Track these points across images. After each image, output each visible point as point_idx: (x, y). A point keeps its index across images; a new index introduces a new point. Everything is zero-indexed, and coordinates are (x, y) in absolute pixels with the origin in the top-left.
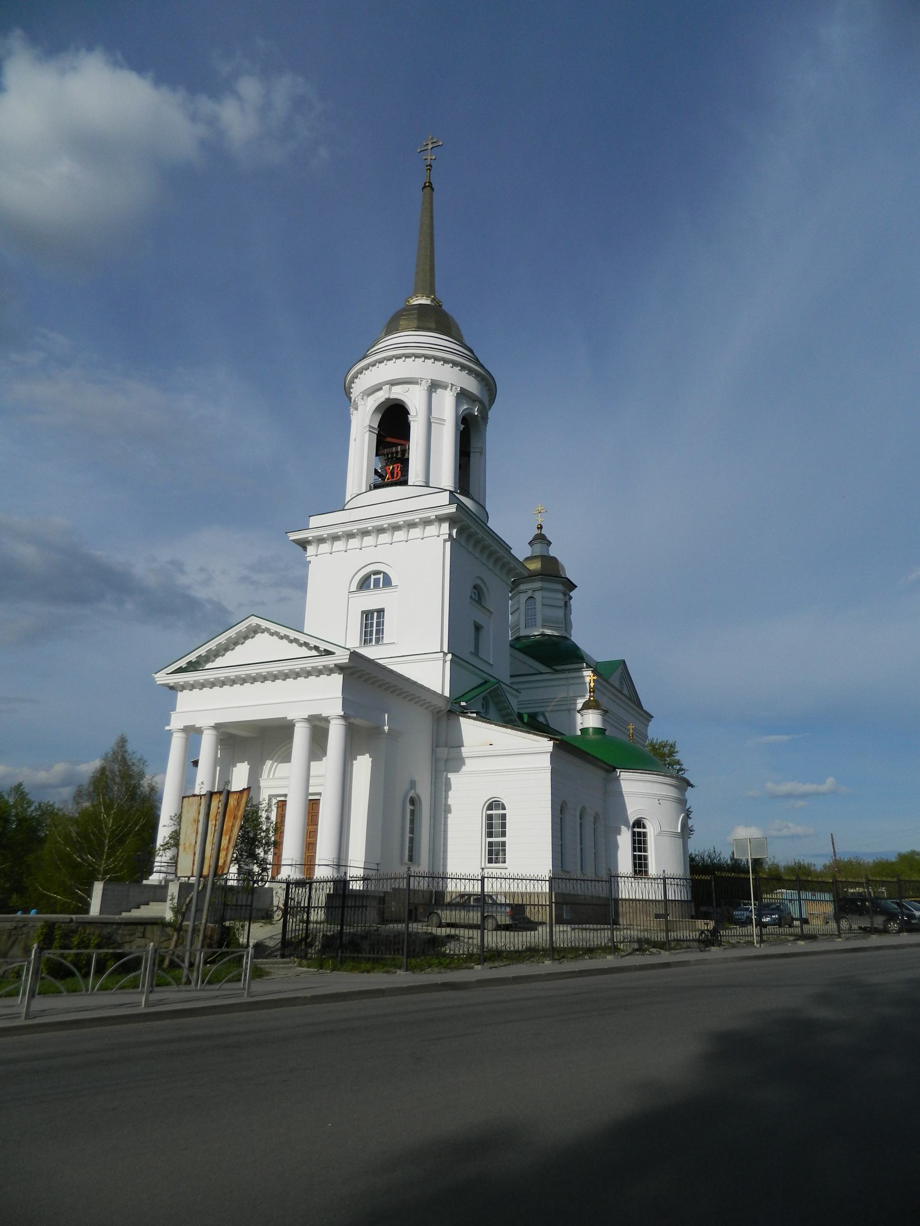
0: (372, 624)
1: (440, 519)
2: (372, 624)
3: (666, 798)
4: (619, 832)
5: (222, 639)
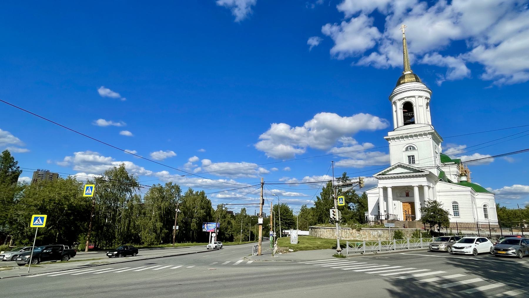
0: (412, 159)
1: (429, 134)
2: (412, 159)
5: (388, 169)
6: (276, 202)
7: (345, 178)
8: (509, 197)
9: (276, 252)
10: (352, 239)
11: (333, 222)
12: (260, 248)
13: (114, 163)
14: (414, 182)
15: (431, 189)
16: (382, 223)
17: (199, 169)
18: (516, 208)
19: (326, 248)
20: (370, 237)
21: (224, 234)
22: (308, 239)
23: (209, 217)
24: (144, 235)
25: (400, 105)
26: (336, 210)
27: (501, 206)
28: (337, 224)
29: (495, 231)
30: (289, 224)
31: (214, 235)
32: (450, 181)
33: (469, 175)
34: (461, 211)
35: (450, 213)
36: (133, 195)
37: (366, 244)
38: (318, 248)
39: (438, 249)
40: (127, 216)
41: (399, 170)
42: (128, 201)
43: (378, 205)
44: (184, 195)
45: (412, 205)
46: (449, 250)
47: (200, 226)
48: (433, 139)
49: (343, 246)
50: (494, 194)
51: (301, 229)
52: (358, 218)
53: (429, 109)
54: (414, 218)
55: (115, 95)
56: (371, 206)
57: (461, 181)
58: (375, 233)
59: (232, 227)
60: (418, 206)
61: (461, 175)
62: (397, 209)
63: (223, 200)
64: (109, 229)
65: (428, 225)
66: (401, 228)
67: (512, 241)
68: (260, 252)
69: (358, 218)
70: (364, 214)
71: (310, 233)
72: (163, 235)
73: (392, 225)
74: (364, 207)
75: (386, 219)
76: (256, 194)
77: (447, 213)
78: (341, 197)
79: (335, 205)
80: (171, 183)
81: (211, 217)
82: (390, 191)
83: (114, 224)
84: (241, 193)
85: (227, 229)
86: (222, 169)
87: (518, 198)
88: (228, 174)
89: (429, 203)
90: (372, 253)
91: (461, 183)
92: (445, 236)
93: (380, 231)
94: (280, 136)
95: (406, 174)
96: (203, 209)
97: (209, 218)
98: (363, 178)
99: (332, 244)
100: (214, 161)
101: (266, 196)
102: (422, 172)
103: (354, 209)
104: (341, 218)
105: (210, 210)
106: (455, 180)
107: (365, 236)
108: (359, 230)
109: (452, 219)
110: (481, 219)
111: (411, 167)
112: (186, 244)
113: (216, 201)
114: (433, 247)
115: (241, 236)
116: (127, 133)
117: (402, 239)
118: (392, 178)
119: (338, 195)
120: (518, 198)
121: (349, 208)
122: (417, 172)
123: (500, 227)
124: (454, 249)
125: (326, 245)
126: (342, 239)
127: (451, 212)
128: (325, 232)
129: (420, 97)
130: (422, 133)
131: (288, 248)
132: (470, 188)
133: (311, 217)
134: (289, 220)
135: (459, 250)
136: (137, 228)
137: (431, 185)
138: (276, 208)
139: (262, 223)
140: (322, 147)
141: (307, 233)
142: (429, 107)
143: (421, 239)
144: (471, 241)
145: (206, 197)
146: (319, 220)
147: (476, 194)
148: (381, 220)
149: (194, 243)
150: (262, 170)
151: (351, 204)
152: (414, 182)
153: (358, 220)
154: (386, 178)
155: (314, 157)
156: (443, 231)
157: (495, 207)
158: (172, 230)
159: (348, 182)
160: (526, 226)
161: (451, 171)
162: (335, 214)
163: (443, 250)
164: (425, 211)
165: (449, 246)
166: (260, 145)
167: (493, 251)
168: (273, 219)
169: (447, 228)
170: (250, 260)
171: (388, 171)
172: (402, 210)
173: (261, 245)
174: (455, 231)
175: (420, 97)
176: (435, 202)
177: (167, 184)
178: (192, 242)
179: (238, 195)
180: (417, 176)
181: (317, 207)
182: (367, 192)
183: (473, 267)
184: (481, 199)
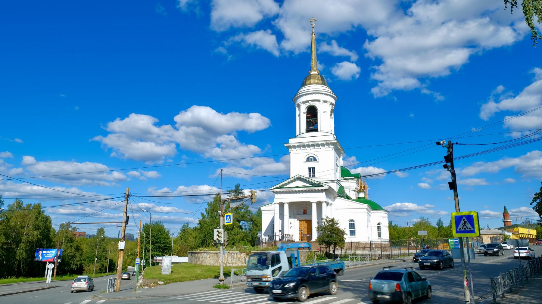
0: (312, 171)
1: (332, 144)
2: (312, 171)
3: (337, 224)
5: (286, 182)
6: (146, 220)
7: (237, 190)
9: (141, 286)
10: (240, 265)
11: (217, 245)
12: (118, 281)
14: (313, 198)
17: (20, 170)
18: (406, 226)
19: (206, 277)
21: (69, 265)
22: (185, 267)
23: (46, 240)
25: (304, 109)
26: (222, 230)
27: (393, 224)
28: (221, 247)
29: (386, 250)
31: (51, 266)
32: (348, 198)
33: (367, 191)
35: (346, 233)
38: (197, 278)
41: (299, 183)
43: (272, 223)
45: (309, 223)
49: (227, 275)
50: (388, 212)
52: (250, 239)
53: (333, 116)
54: (311, 238)
56: (265, 225)
57: (359, 198)
59: (81, 255)
60: (315, 225)
61: (359, 191)
62: (293, 228)
63: (66, 217)
65: (324, 246)
76: (116, 209)
77: (343, 232)
78: (229, 214)
79: (221, 224)
81: (49, 240)
82: (286, 207)
84: (92, 207)
85: (73, 257)
87: (405, 215)
89: (326, 221)
91: (359, 200)
94: (135, 131)
96: (37, 229)
97: (47, 242)
98: (256, 192)
99: (215, 271)
100: (39, 159)
102: (322, 186)
103: (246, 229)
104: (226, 240)
105: (49, 231)
106: (353, 197)
109: (348, 239)
110: (375, 239)
111: (311, 181)
112: (6, 280)
113: (58, 217)
115: (95, 266)
118: (290, 192)
119: (226, 211)
120: (405, 215)
121: (241, 227)
122: (316, 186)
123: (391, 246)
125: (206, 274)
126: (228, 265)
127: (347, 231)
128: (208, 258)
129: (325, 102)
130: (325, 142)
131: (157, 280)
132: (366, 206)
133: (192, 239)
134: (163, 243)
137: (330, 201)
138: (146, 228)
139: (123, 248)
140: (196, 148)
141: (185, 259)
142: (333, 114)
145: (43, 212)
147: (372, 212)
148: (275, 241)
149: (21, 279)
150: (116, 175)
151: (242, 223)
152: (313, 198)
153: (250, 242)
154: (283, 193)
156: (338, 252)
157: (388, 225)
159: (241, 195)
160: (412, 244)
161: (350, 186)
164: (322, 230)
166: (110, 141)
168: (142, 243)
170: (101, 299)
171: (286, 184)
172: (298, 230)
174: (349, 252)
175: (325, 102)
176: (333, 220)
179: (88, 210)
180: (315, 191)
181: (201, 228)
182: (262, 208)
183: (360, 290)
184: (381, 217)
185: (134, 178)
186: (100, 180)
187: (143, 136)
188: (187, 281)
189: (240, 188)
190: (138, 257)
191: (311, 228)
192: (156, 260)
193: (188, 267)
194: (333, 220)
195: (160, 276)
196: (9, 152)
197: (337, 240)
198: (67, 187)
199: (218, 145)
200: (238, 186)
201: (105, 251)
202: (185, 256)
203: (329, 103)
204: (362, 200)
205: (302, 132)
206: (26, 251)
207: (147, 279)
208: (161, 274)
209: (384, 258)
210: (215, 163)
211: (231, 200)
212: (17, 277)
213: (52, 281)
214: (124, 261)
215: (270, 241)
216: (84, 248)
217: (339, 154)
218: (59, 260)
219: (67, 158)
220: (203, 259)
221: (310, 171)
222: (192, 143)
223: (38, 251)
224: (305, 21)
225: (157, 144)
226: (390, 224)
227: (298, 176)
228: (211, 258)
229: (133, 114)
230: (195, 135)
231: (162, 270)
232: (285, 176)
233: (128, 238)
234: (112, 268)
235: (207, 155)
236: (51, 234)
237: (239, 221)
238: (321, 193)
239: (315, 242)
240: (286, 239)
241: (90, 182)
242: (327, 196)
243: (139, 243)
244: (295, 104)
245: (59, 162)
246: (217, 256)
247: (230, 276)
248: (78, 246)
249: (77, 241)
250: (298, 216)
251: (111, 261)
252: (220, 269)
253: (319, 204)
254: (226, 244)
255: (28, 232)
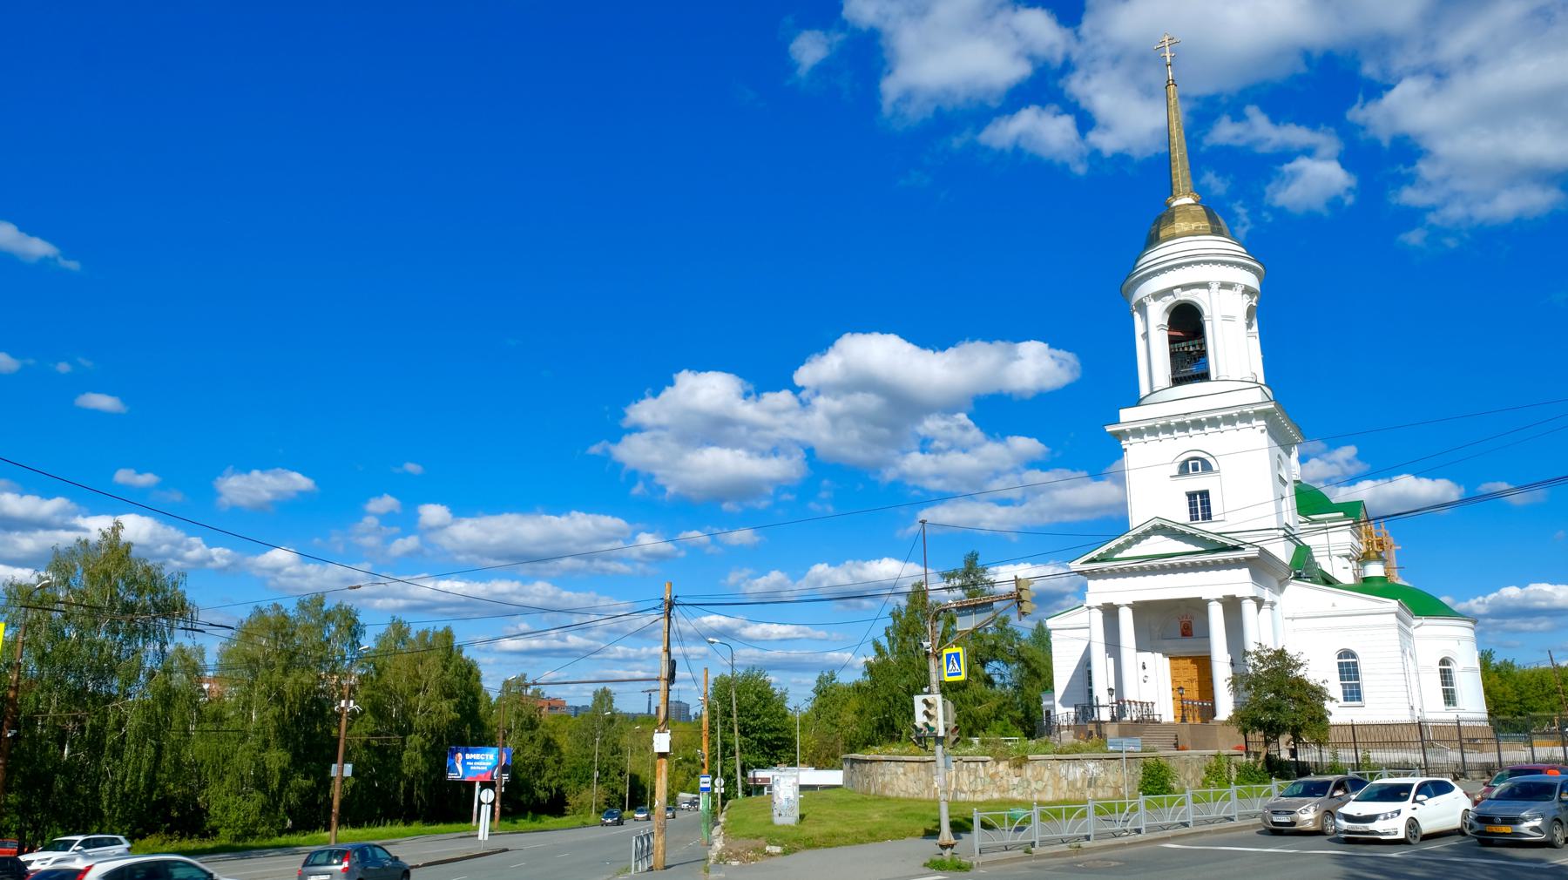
0: (1200, 503)
1: (1259, 415)
2: (1200, 503)
4: (13, 355)
5: (1121, 541)
6: (720, 668)
7: (971, 575)
8: (1511, 623)
9: (720, 858)
10: (996, 796)
12: (657, 841)
13: (80, 521)
14: (1210, 586)
15: (1265, 610)
16: (1100, 735)
17: (411, 542)
18: (1546, 664)
19: (899, 835)
20: (1057, 787)
21: (530, 790)
22: (838, 803)
23: (471, 726)
24: (219, 800)
25: (1158, 314)
26: (937, 699)
27: (1497, 660)
28: (939, 747)
30: (774, 748)
32: (1328, 581)
34: (1367, 682)
35: (1331, 693)
36: (170, 648)
37: (1044, 816)
38: (873, 836)
39: (1293, 824)
40: (145, 733)
42: (152, 675)
43: (1085, 669)
44: (373, 645)
45: (1204, 664)
46: (1330, 829)
47: (439, 754)
48: (1271, 434)
51: (818, 763)
52: (1019, 714)
53: (1255, 328)
54: (1211, 712)
55: (38, 248)
56: (1063, 672)
57: (1365, 579)
58: (1076, 772)
59: (559, 762)
60: (1222, 671)
61: (1364, 559)
62: (1151, 682)
63: (524, 659)
64: (73, 784)
65: (1258, 736)
66: (1165, 752)
67: (1531, 787)
68: (660, 857)
69: (1019, 714)
70: (1039, 701)
71: (847, 779)
72: (293, 798)
73: (1132, 745)
74: (1039, 676)
75: (1113, 719)
76: (641, 633)
77: (1318, 694)
78: (955, 650)
79: (934, 678)
80: (319, 600)
82: (1126, 619)
83: (98, 764)
85: (539, 768)
86: (493, 541)
88: (522, 560)
89: (1260, 659)
90: (1064, 848)
91: (1366, 586)
92: (1312, 778)
93: (1091, 765)
94: (701, 419)
95: (1188, 560)
96: (449, 696)
99: (924, 817)
100: (461, 509)
101: (681, 641)
102: (1236, 548)
103: (1004, 686)
104: (952, 726)
105: (476, 700)
107: (1040, 785)
108: (1020, 763)
109: (1339, 713)
110: (1435, 711)
114: (1276, 819)
115: (594, 794)
116: (103, 402)
117: (1170, 791)
118: (1133, 573)
119: (944, 640)
121: (989, 681)
122: (1217, 552)
124: (1344, 825)
125: (899, 824)
126: (961, 797)
127: (1335, 688)
128: (900, 777)
129: (1226, 286)
131: (762, 841)
132: (1394, 605)
133: (851, 717)
134: (770, 731)
135: (1360, 827)
136: (194, 774)
137: (1267, 595)
138: (722, 690)
139: (667, 750)
140: (860, 455)
141: (834, 777)
142: (1255, 322)
143: (1234, 788)
144: (1395, 793)
146: (880, 728)
147: (1416, 622)
148: (1099, 723)
149: (416, 826)
150: (648, 541)
151: (992, 668)
152: (1210, 586)
154: (1113, 574)
155: (845, 495)
156: (1308, 756)
157: (1478, 666)
158: (325, 782)
162: (931, 711)
163: (1310, 826)
165: (1330, 813)
166: (632, 451)
167: (1471, 827)
168: (712, 730)
169: (1320, 744)
171: (1120, 548)
173: (663, 830)
174: (1347, 756)
175: (1226, 286)
176: (1281, 654)
177: (302, 606)
178: (407, 822)
179: (574, 640)
180: (1216, 566)
181: (874, 682)
182: (1050, 623)
184: (1453, 641)
185: (696, 550)
186: (607, 558)
187: (717, 430)
188: (847, 844)
189: (979, 563)
190: (705, 771)
191: (1211, 680)
192: (755, 780)
193: (847, 803)
194: (1281, 654)
195: (768, 829)
196: (392, 494)
197: (1301, 719)
198: (525, 581)
199: (925, 445)
200: (972, 560)
201: (617, 751)
202: (832, 767)
203: (1240, 289)
204: (1378, 585)
205: (1158, 384)
206: (424, 753)
207: (736, 838)
208: (771, 823)
209: (1476, 775)
210: (907, 497)
211: (958, 609)
212: (408, 821)
213: (492, 833)
214: (671, 779)
215: (1081, 722)
216: (565, 743)
217: (1286, 446)
218: (505, 777)
219: (524, 505)
220: (887, 778)
221: (1192, 504)
222: (847, 444)
223: (454, 753)
224: (1140, 65)
225: (751, 450)
226: (1485, 660)
227: (1157, 523)
228: (911, 776)
229: (685, 372)
230: (857, 416)
231: (776, 813)
232: (1114, 522)
233: (676, 715)
234: (638, 796)
235: (890, 475)
236: (482, 710)
237: (983, 664)
238: (1234, 572)
239: (1225, 723)
240: (1132, 715)
241: (583, 563)
242: (1257, 577)
243: (705, 733)
244: (1128, 302)
245: (506, 516)
246: (928, 770)
247: (968, 831)
248: (548, 740)
249: (545, 726)
250: (1166, 643)
251: (634, 779)
252: (938, 809)
253: (1232, 606)
254: (953, 738)
255: (429, 702)
